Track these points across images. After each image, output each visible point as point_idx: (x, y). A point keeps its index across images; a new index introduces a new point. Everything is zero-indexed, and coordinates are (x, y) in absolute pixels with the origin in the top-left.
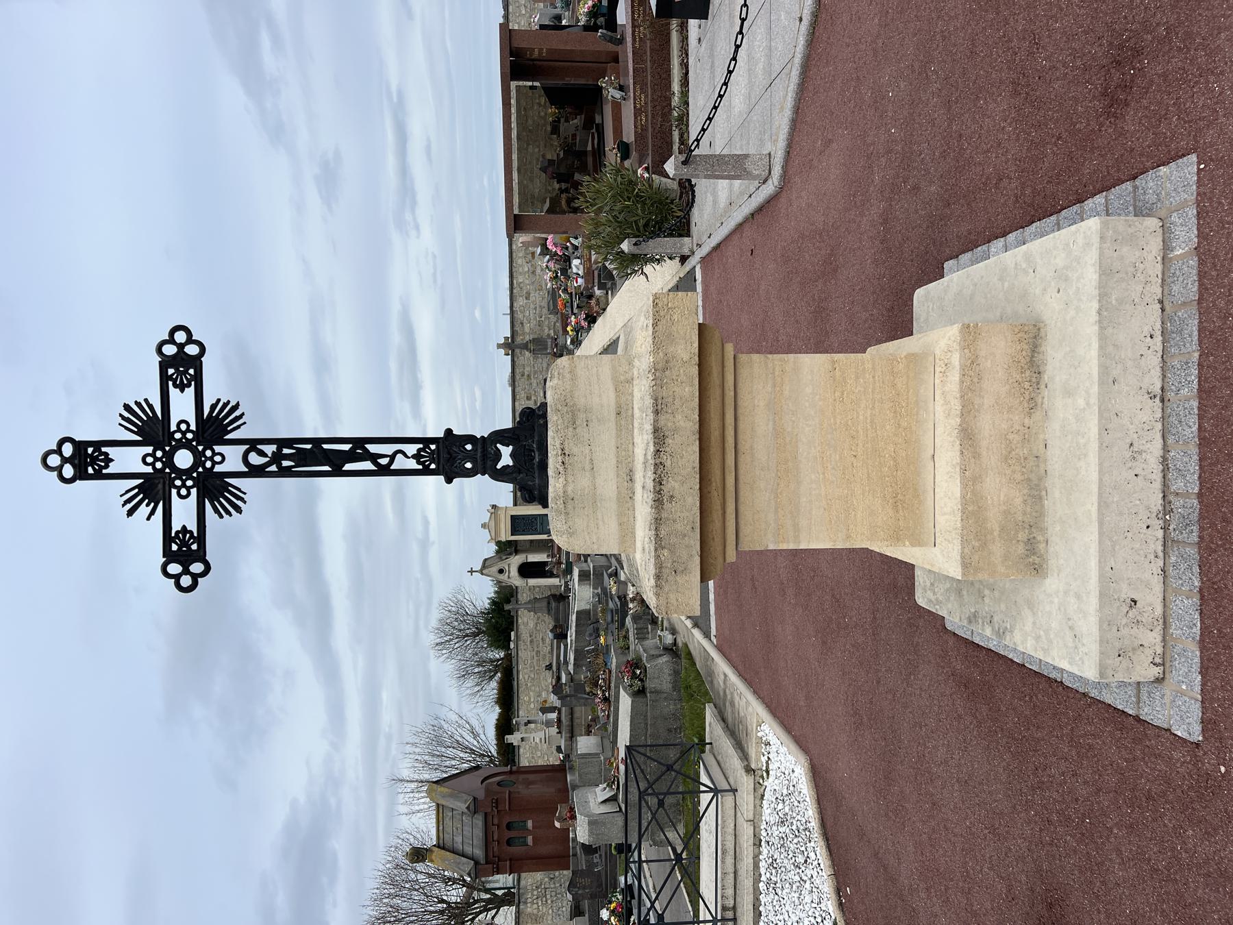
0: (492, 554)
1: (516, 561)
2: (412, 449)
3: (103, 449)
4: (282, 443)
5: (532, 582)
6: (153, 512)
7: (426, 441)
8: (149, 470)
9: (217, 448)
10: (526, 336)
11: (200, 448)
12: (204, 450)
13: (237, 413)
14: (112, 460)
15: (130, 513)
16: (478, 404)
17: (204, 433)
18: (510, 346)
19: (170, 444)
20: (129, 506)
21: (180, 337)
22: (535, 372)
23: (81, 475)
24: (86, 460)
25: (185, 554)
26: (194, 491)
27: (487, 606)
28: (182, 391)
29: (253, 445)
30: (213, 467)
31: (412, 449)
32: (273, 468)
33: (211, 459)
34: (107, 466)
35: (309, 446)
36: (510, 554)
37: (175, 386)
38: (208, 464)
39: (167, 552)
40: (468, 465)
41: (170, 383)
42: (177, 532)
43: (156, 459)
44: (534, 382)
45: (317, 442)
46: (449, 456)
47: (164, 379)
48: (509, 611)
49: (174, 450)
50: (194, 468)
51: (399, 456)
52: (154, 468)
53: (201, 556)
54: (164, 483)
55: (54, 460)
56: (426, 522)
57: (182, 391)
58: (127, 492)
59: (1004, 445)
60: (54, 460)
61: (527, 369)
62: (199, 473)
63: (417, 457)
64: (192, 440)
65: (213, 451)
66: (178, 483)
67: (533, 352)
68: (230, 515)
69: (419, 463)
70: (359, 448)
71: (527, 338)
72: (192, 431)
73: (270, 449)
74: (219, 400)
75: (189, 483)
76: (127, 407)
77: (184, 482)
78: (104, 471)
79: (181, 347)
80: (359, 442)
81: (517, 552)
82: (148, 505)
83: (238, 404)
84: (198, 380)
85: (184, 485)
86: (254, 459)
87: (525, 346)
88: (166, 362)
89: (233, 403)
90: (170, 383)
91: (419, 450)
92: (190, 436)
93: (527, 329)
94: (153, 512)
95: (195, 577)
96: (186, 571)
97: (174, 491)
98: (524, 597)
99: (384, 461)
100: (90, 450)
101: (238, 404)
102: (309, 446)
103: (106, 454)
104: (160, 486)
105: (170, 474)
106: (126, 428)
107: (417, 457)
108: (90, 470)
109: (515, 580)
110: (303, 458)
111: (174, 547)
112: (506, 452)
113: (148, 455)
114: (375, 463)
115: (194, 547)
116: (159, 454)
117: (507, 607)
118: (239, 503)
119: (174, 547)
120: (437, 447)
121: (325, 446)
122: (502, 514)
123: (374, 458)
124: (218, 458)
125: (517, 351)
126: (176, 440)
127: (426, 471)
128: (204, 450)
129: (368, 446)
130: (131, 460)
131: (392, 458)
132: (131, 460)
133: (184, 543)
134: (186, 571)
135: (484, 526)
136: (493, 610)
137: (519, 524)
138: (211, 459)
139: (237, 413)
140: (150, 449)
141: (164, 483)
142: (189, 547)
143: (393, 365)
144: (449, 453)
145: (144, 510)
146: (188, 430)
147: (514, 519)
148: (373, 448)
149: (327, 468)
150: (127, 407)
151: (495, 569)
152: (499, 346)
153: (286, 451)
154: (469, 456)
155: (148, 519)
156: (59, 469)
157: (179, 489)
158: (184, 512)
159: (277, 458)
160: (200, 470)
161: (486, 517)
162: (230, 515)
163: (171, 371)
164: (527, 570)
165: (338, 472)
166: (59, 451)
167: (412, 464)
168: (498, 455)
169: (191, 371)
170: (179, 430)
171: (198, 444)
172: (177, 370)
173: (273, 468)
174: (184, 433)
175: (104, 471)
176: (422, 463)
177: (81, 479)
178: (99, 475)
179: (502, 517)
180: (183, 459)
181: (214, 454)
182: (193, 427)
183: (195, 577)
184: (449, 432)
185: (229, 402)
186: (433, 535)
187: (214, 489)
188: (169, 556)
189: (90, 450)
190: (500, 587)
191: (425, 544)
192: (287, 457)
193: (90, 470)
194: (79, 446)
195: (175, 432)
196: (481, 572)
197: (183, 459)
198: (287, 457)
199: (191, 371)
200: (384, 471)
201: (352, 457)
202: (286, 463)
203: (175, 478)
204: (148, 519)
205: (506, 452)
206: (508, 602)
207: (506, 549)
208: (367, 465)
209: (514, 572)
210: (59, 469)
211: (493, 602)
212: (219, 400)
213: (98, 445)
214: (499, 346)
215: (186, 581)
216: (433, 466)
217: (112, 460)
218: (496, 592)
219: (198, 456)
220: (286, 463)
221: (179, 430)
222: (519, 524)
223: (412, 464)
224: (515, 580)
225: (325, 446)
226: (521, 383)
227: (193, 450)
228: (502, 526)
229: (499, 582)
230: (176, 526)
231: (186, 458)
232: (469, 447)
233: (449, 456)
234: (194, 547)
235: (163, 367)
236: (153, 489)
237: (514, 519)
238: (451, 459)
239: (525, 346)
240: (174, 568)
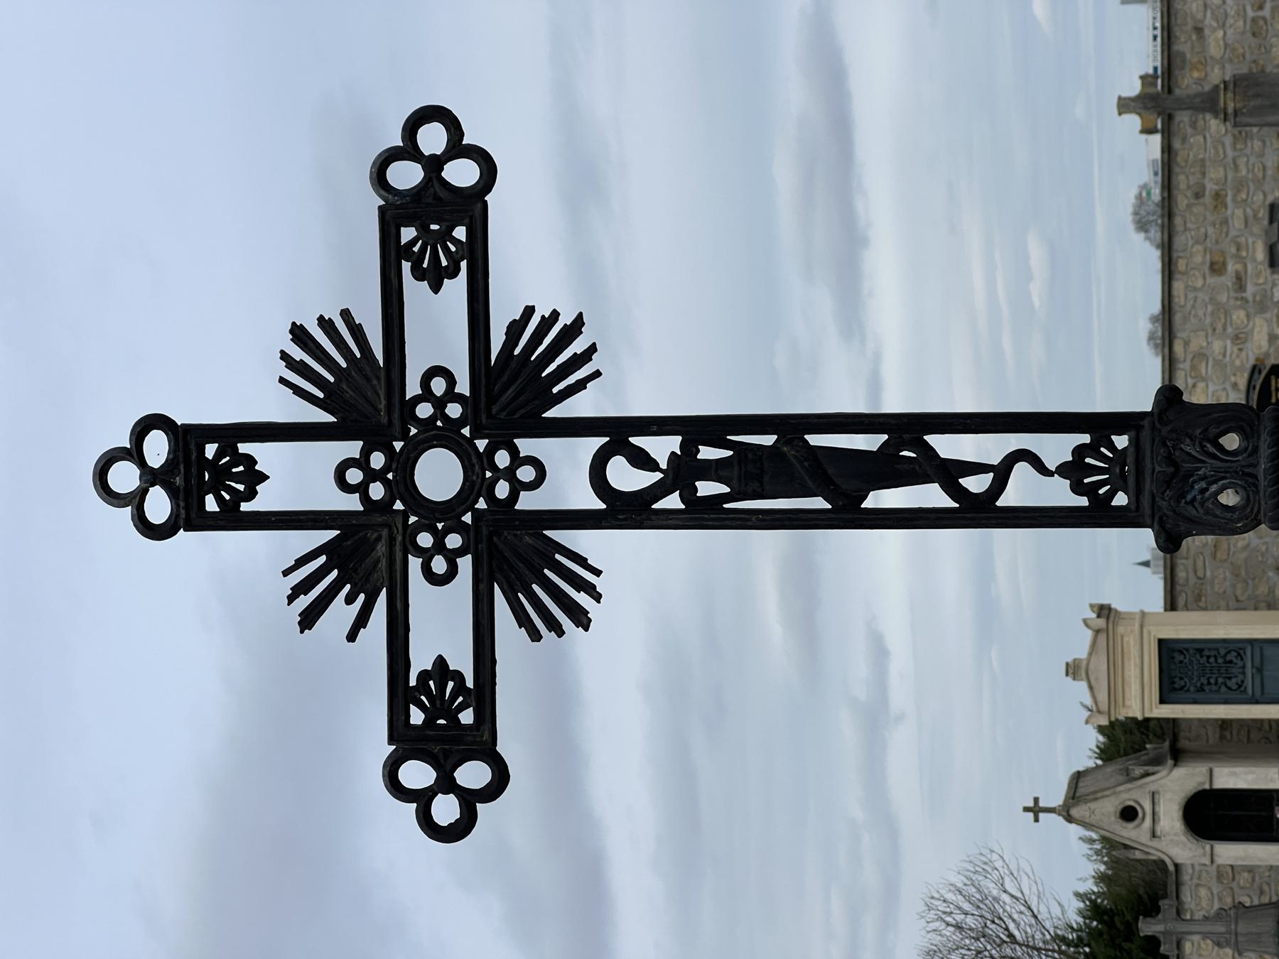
0: (1086, 759)
1: (1175, 784)
2: (1057, 448)
3: (244, 448)
4: (697, 429)
5: (1231, 852)
6: (362, 620)
7: (1099, 425)
9: (526, 446)
10: (1212, 66)
11: (481, 444)
12: (491, 451)
13: (578, 347)
14: (263, 477)
15: (308, 619)
16: (1037, 291)
17: (491, 400)
18: (1160, 103)
19: (404, 436)
20: (304, 601)
22: (1240, 185)
23: (189, 517)
27: (1075, 920)
29: (619, 434)
31: (1057, 448)
32: (673, 502)
33: (510, 475)
34: (251, 494)
35: (768, 440)
36: (1157, 761)
37: (419, 274)
38: (502, 490)
39: (398, 729)
40: (1229, 498)
41: (406, 266)
42: (424, 676)
44: (1236, 216)
45: (792, 427)
48: (1153, 942)
49: (416, 450)
50: (464, 499)
51: (1022, 470)
52: (365, 498)
54: (392, 540)
55: (125, 477)
56: (880, 652)
58: (301, 562)
61: (1215, 173)
62: (477, 515)
63: (1073, 471)
64: (461, 422)
65: (514, 452)
66: (425, 540)
67: (1235, 119)
68: (560, 632)
69: (1077, 489)
70: (907, 443)
71: (1216, 76)
73: (662, 448)
74: (529, 311)
75: (453, 541)
76: (299, 334)
77: (439, 538)
79: (434, 165)
80: (910, 429)
81: (1177, 755)
82: (350, 600)
83: (579, 323)
85: (439, 547)
86: (625, 477)
87: (1208, 103)
89: (566, 319)
90: (406, 266)
91: (1079, 451)
92: (454, 410)
93: (1214, 47)
94: (362, 620)
95: (470, 800)
96: (446, 784)
97: (415, 563)
98: (1200, 899)
99: (976, 484)
100: (210, 450)
101: (579, 323)
102: (768, 440)
103: (250, 461)
104: (381, 549)
105: (405, 515)
106: (298, 391)
107: (1073, 471)
108: (211, 504)
109: (1169, 839)
110: (751, 473)
111: (417, 717)
114: (954, 489)
115: (467, 717)
116: (378, 460)
117: (1147, 927)
118: (582, 599)
119: (417, 717)
120: (1135, 442)
121: (815, 440)
122: (1129, 637)
123: (949, 474)
125: (1183, 118)
127: (1098, 515)
128: (491, 451)
129: (932, 439)
131: (1002, 473)
133: (440, 707)
134: (446, 784)
135: (1073, 670)
136: (1094, 935)
137: (1183, 667)
139: (578, 347)
140: (352, 448)
141: (392, 540)
142: (453, 718)
143: (784, 176)
144: (1170, 460)
145: (341, 613)
146: (451, 395)
147: (1167, 649)
148: (947, 446)
149: (819, 503)
150: (299, 334)
151: (1107, 809)
152: (1124, 106)
153: (707, 453)
155: (352, 637)
158: (441, 622)
159: (683, 472)
160: (481, 504)
161: (1079, 644)
162: (560, 632)
163: (408, 234)
164: (1212, 815)
167: (1059, 493)
169: (460, 233)
170: (427, 395)
171: (476, 434)
172: (423, 229)
173: (673, 502)
174: (440, 404)
176: (1089, 491)
177: (190, 527)
178: (232, 519)
179: (1131, 643)
180: (439, 475)
181: (518, 460)
182: (463, 387)
183: (470, 800)
185: (555, 315)
186: (900, 696)
189: (210, 450)
190: (1114, 863)
191: (875, 718)
194: (186, 439)
196: (1066, 812)
197: (439, 475)
199: (460, 233)
200: (979, 512)
201: (887, 470)
202: (706, 488)
203: (418, 528)
204: (352, 637)
206: (1152, 909)
207: (1129, 743)
208: (932, 496)
209: (1171, 819)
210: (136, 500)
211: (1094, 910)
213: (231, 435)
214: (1124, 106)
215: (446, 810)
216: (1121, 499)
217: (263, 477)
218: (1101, 878)
220: (706, 488)
221: (427, 395)
222: (1183, 667)
223: (1059, 493)
224: (1169, 839)
225: (815, 440)
226: (1194, 223)
227: (463, 450)
228: (1132, 672)
229: (1110, 847)
234: (467, 717)
235: (389, 223)
237: (1167, 649)
238: (1178, 478)
239: (1208, 103)
240: (417, 774)
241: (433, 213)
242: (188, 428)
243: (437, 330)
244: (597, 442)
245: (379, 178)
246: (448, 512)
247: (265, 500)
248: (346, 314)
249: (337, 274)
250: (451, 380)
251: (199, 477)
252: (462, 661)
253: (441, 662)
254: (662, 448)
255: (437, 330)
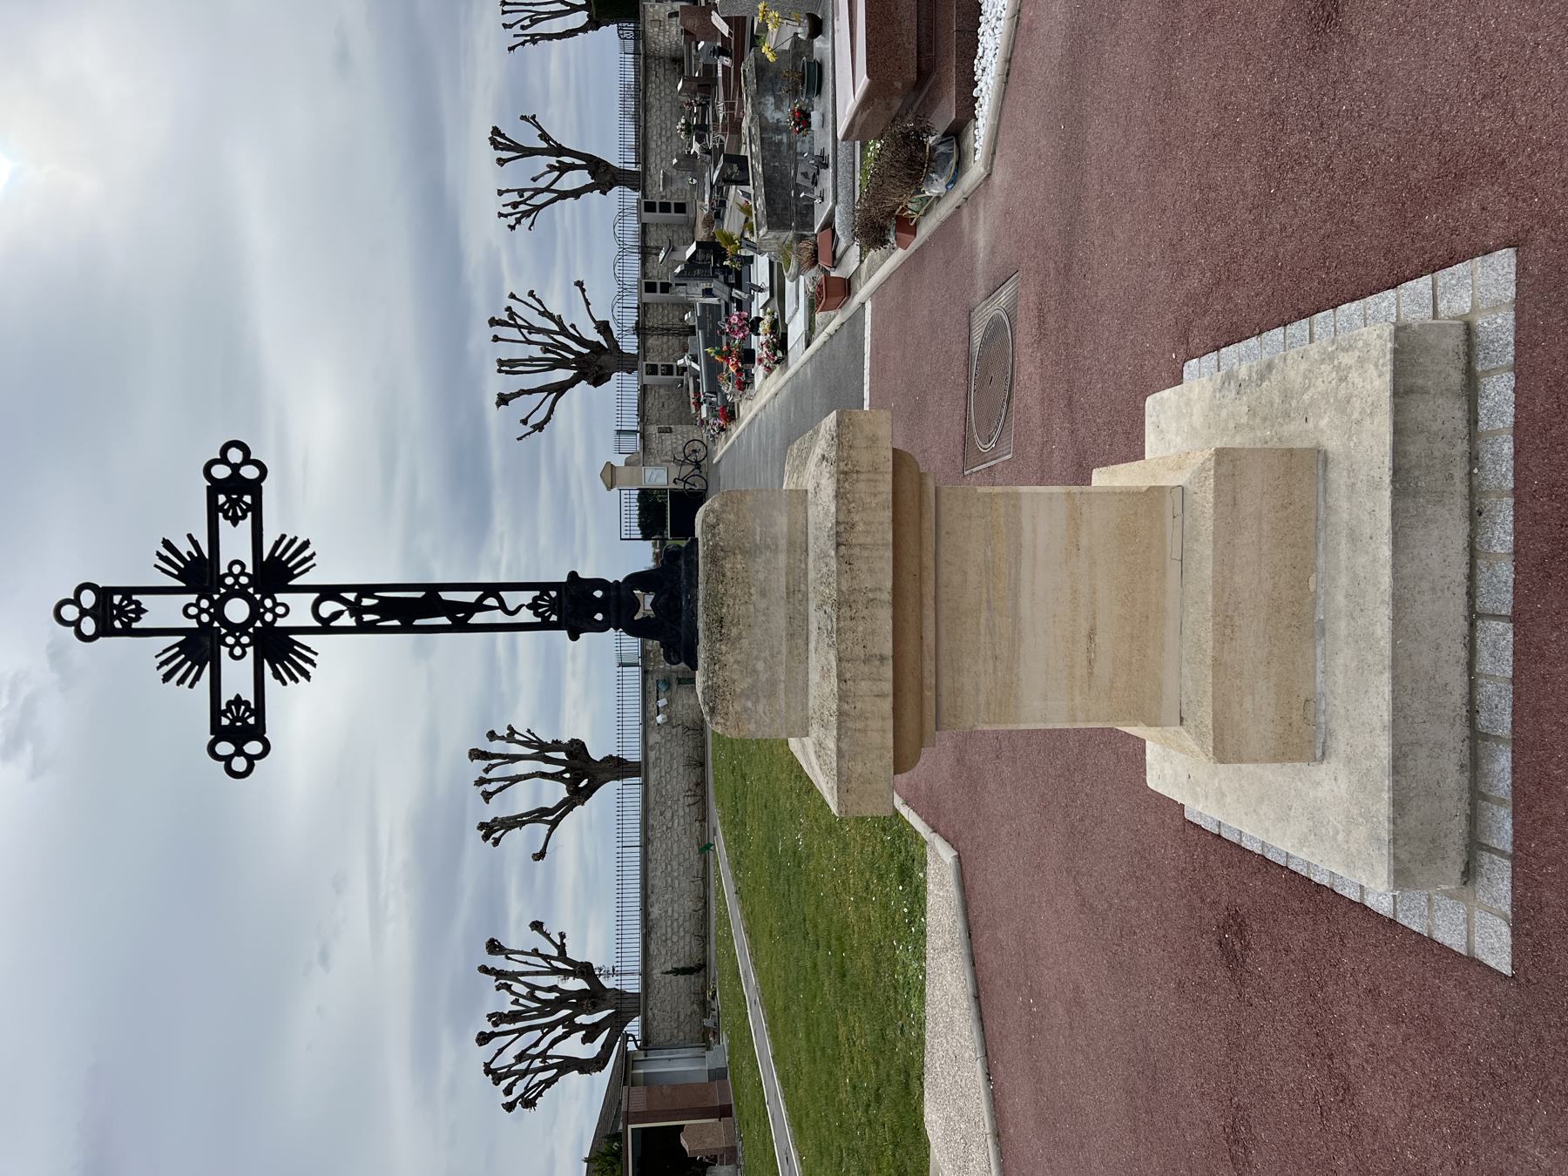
2: (527, 597)
3: (135, 597)
4: (365, 590)
7: (544, 587)
8: (193, 624)
9: (280, 597)
13: (306, 553)
21: (239, 764)
24: (111, 612)
25: (235, 490)
26: (224, 570)
28: (238, 697)
29: (329, 592)
30: (274, 620)
31: (527, 597)
35: (419, 595)
39: (215, 727)
40: (599, 617)
42: (244, 517)
43: (272, 610)
46: (572, 606)
47: (213, 510)
50: (250, 622)
52: (199, 621)
53: (258, 732)
55: (70, 613)
57: (238, 697)
58: (165, 651)
59: (1225, 595)
60: (70, 613)
62: (256, 629)
63: (533, 606)
65: (274, 600)
68: (297, 681)
69: (537, 614)
72: (247, 575)
75: (245, 640)
77: (237, 582)
78: (135, 625)
84: (256, 509)
85: (236, 577)
88: (215, 487)
103: (138, 603)
106: (308, 649)
107: (533, 606)
111: (225, 722)
112: (647, 601)
113: (282, 616)
115: (251, 721)
118: (307, 667)
119: (247, 499)
124: (280, 610)
126: (248, 634)
127: (546, 625)
130: (167, 611)
132: (167, 611)
134: (239, 752)
138: (272, 610)
142: (229, 499)
148: (446, 596)
149: (396, 623)
153: (366, 602)
154: (600, 605)
156: (76, 624)
157: (243, 573)
162: (297, 681)
165: (461, 626)
166: (76, 601)
167: (526, 616)
168: (636, 605)
175: (135, 625)
180: (237, 610)
181: (197, 617)
182: (249, 570)
183: (251, 759)
184: (573, 575)
187: (277, 650)
188: (219, 734)
192: (369, 610)
193: (117, 624)
194: (104, 594)
195: (226, 575)
197: (237, 610)
198: (369, 610)
202: (367, 618)
205: (647, 601)
212: (191, 686)
213: (127, 592)
216: (554, 618)
219: (218, 614)
220: (367, 618)
230: (246, 524)
231: (228, 610)
232: (598, 594)
233: (572, 606)
234: (251, 721)
236: (198, 649)
241: (235, 490)
242: (105, 588)
243: (235, 544)
244: (316, 595)
245: (267, 747)
246: (232, 593)
247: (144, 623)
248: (284, 683)
249: (187, 522)
250: (243, 566)
251: (111, 612)
252: (224, 524)
253: (235, 524)
254: (351, 596)
255: (235, 544)
